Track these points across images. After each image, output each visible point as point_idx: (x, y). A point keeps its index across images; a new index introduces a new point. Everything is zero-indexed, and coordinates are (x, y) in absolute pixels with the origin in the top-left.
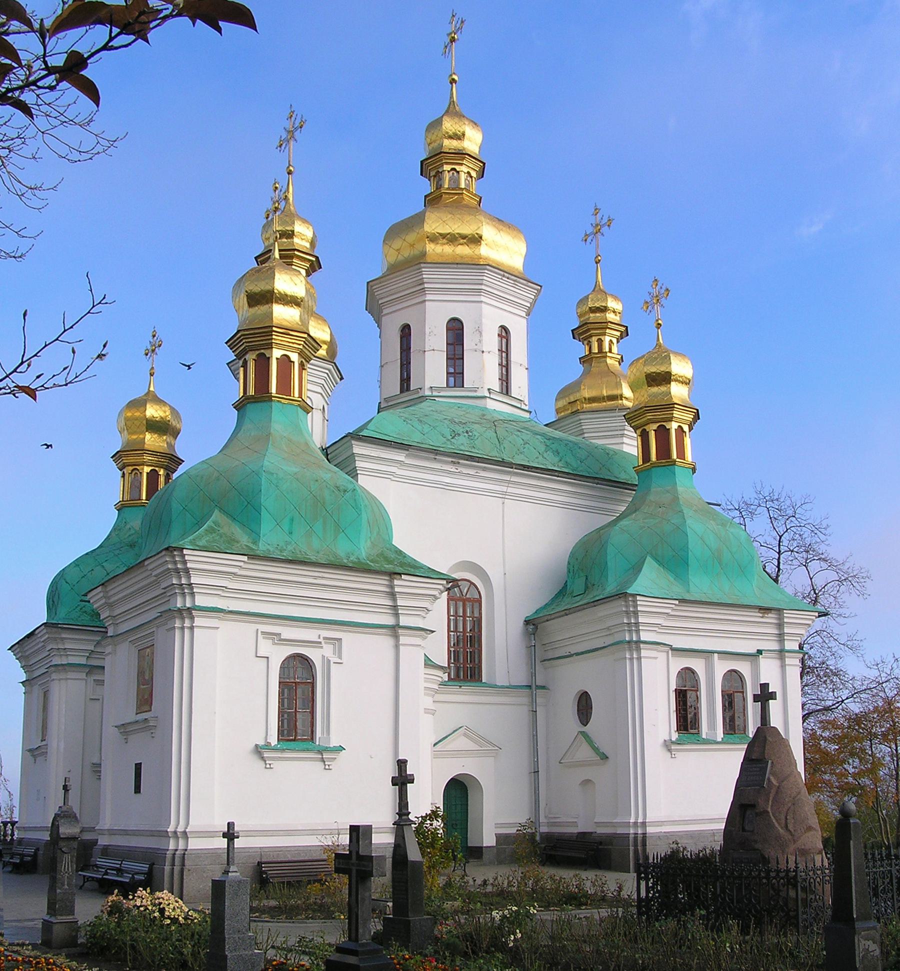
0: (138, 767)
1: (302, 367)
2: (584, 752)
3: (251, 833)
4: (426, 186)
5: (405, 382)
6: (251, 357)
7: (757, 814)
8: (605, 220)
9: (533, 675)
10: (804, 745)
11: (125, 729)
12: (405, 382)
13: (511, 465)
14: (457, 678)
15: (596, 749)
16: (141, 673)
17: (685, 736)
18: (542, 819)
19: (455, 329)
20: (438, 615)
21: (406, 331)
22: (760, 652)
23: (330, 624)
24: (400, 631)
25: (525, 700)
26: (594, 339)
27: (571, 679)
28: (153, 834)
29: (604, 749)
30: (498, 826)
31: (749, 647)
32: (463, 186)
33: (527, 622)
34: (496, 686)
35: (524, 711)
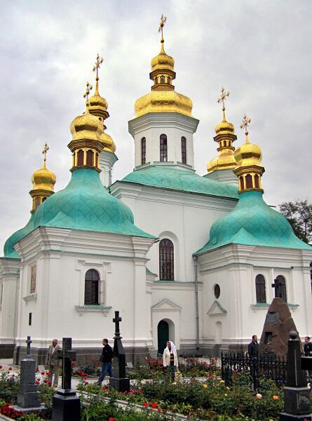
0: (30, 314)
1: (97, 155)
2: (217, 310)
3: (36, 342)
4: (152, 83)
5: (143, 160)
6: (77, 151)
7: (273, 337)
8: (227, 93)
9: (196, 277)
10: (167, 156)
11: (26, 299)
12: (143, 160)
13: (185, 192)
14: (163, 280)
15: (222, 309)
16: (32, 277)
17: (259, 304)
18: (200, 338)
19: (164, 140)
20: (154, 253)
21: (143, 140)
22: (292, 267)
23: (106, 256)
24: (135, 259)
25: (193, 288)
26: (222, 141)
27: (210, 280)
28: (242, 333)
29: (224, 308)
30: (181, 340)
31: (288, 266)
32: (166, 82)
33: (193, 256)
34: (180, 283)
35: (193, 293)
